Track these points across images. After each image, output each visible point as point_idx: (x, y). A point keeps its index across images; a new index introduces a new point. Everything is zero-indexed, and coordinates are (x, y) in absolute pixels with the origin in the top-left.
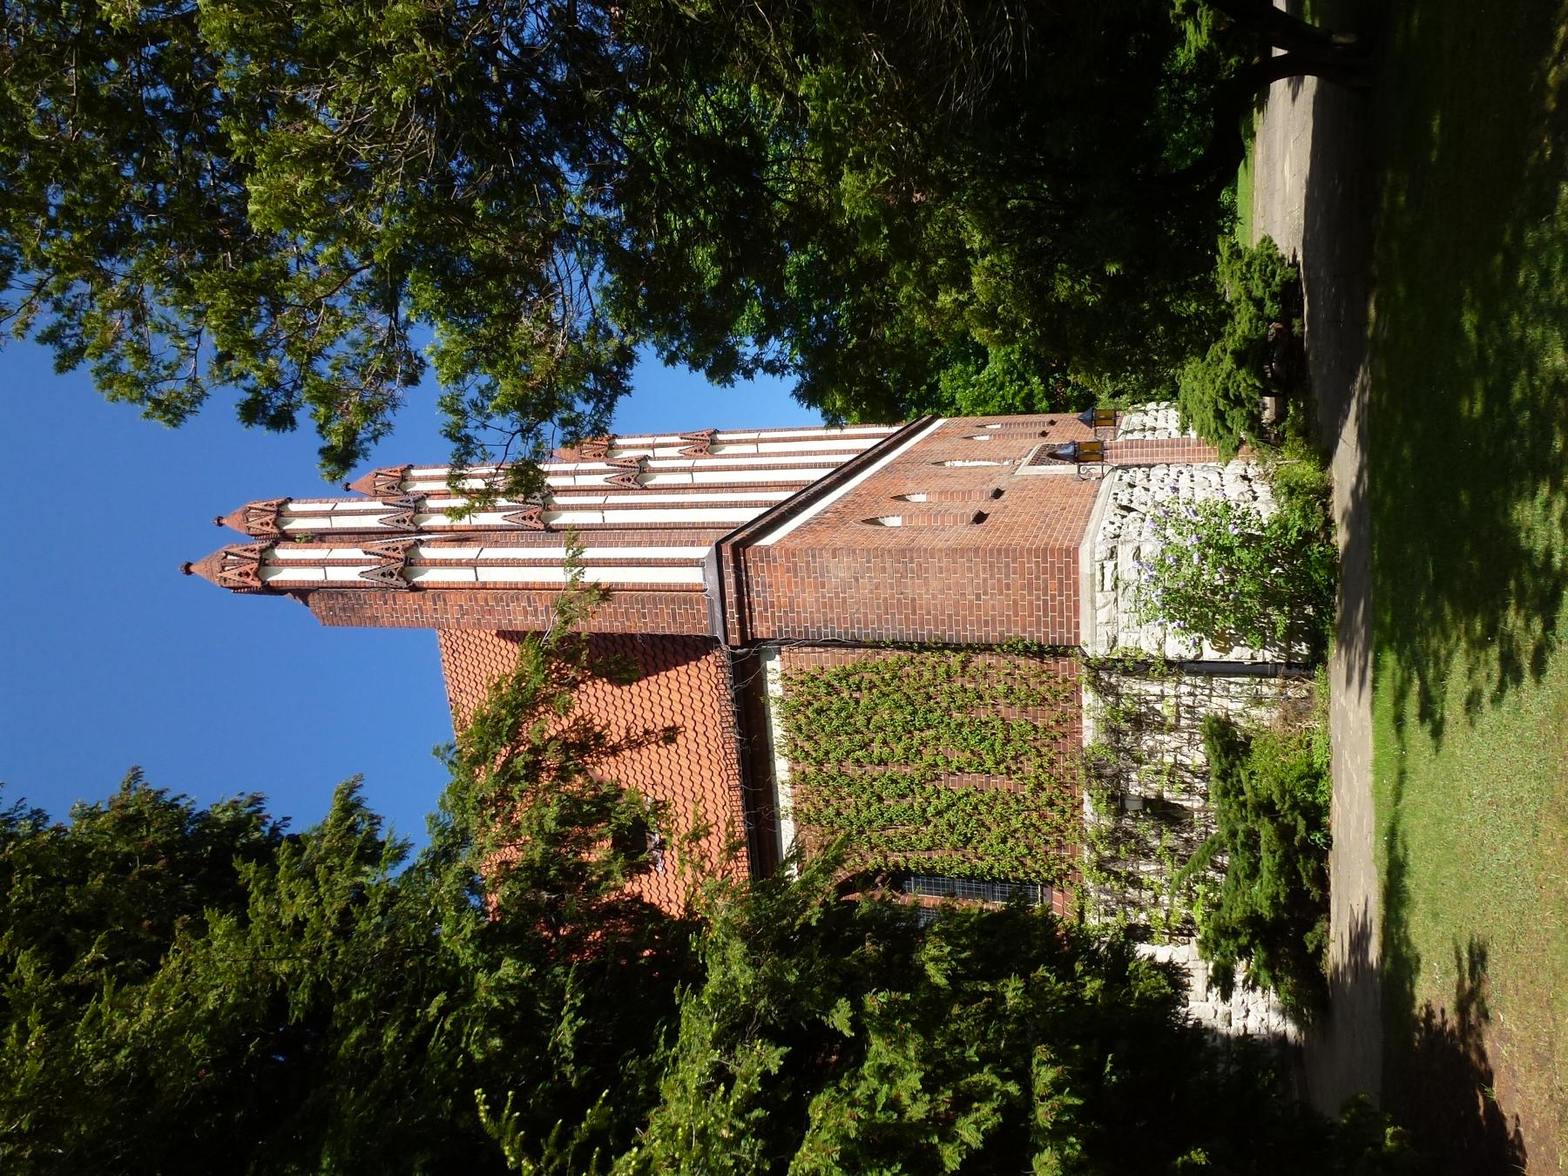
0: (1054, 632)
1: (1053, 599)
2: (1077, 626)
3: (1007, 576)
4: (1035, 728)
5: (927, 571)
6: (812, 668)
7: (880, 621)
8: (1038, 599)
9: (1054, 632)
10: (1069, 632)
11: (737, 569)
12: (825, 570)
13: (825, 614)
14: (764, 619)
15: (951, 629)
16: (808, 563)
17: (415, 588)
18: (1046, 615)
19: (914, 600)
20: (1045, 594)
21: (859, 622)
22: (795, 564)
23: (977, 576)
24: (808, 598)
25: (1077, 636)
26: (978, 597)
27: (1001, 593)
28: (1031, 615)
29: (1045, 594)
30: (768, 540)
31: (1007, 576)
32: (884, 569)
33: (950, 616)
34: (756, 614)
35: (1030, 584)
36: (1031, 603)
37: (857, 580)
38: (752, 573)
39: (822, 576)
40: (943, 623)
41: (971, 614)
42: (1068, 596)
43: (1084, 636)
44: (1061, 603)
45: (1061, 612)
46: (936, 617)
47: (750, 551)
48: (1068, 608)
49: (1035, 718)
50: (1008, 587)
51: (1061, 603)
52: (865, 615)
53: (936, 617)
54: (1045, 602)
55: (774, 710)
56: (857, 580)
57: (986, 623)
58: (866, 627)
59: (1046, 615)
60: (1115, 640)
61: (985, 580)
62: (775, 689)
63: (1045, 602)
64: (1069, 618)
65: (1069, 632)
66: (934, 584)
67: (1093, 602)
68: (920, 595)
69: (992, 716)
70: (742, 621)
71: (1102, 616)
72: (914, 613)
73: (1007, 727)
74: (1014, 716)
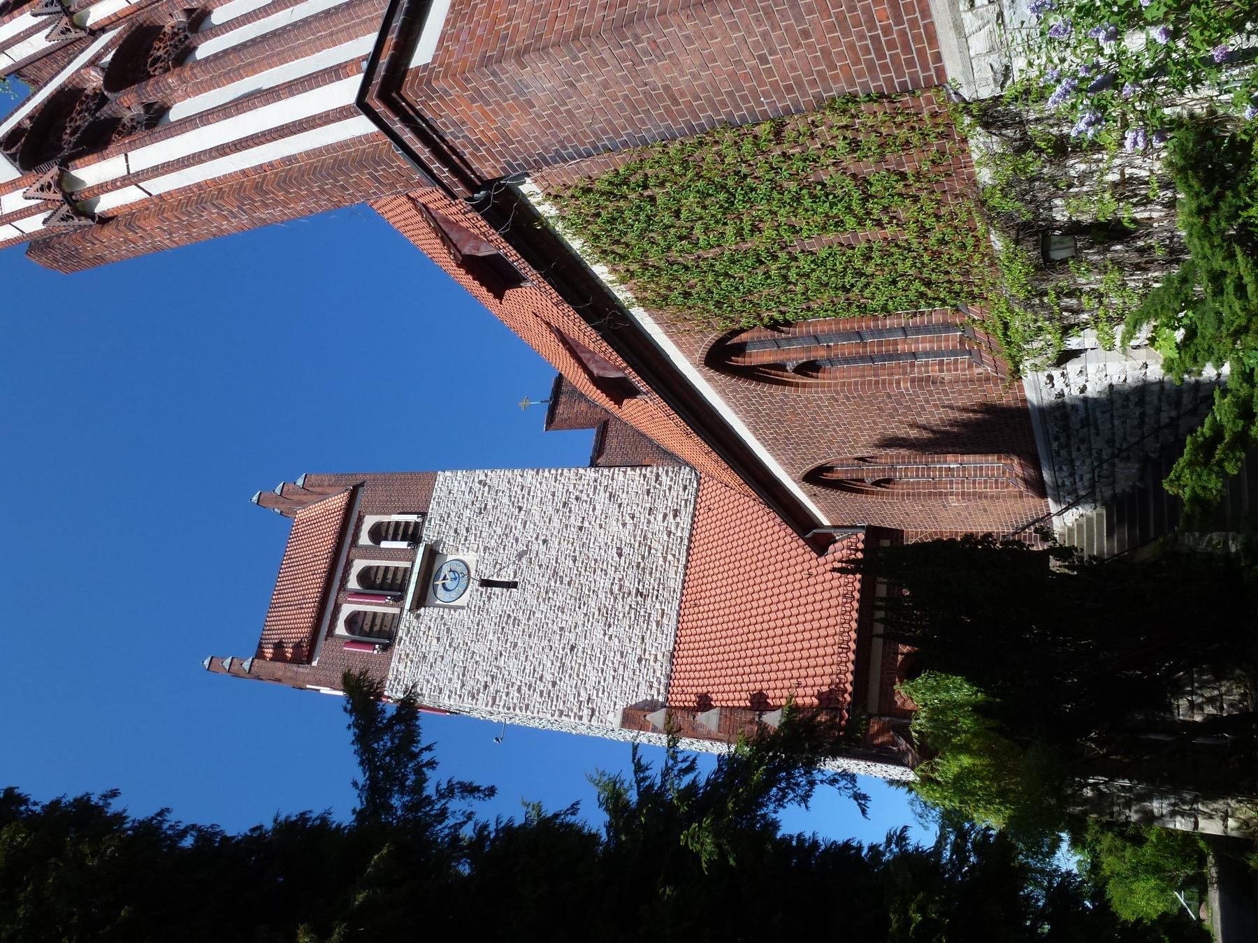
0: (900, 74)
1: (887, 30)
2: (938, 57)
3: (799, 20)
4: (903, 176)
5: (667, 46)
6: (577, 180)
7: (633, 124)
8: (862, 37)
9: (900, 74)
10: (925, 68)
11: (407, 120)
12: (521, 88)
13: (554, 135)
14: (482, 159)
15: (738, 108)
16: (491, 84)
17: (104, 220)
18: (881, 56)
19: (667, 88)
20: (872, 27)
21: (605, 132)
22: (476, 90)
23: (750, 32)
24: (520, 123)
25: (941, 72)
26: (554, 684)
27: (798, 45)
28: (857, 62)
29: (872, 27)
30: (423, 53)
31: (799, 20)
32: (603, 62)
33: (730, 94)
34: (467, 157)
35: (841, 20)
36: (851, 47)
37: (572, 85)
38: (428, 115)
39: (522, 93)
40: (725, 105)
41: (761, 83)
42: (913, 23)
43: (953, 70)
44: (903, 34)
45: (906, 48)
46: (710, 100)
47: (408, 92)
48: (917, 39)
49: (901, 164)
50: (806, 34)
51: (903, 34)
52: (609, 122)
53: (710, 100)
54: (875, 39)
55: (559, 227)
56: (572, 85)
57: (789, 89)
58: (618, 134)
59: (881, 56)
60: (1007, 69)
61: (765, 35)
62: (547, 210)
63: (875, 39)
64: (921, 52)
65: (925, 68)
66: (686, 60)
67: (958, 27)
68: (676, 82)
69: (838, 176)
70: (455, 170)
71: (978, 44)
72: (676, 102)
73: (862, 182)
74: (868, 167)
